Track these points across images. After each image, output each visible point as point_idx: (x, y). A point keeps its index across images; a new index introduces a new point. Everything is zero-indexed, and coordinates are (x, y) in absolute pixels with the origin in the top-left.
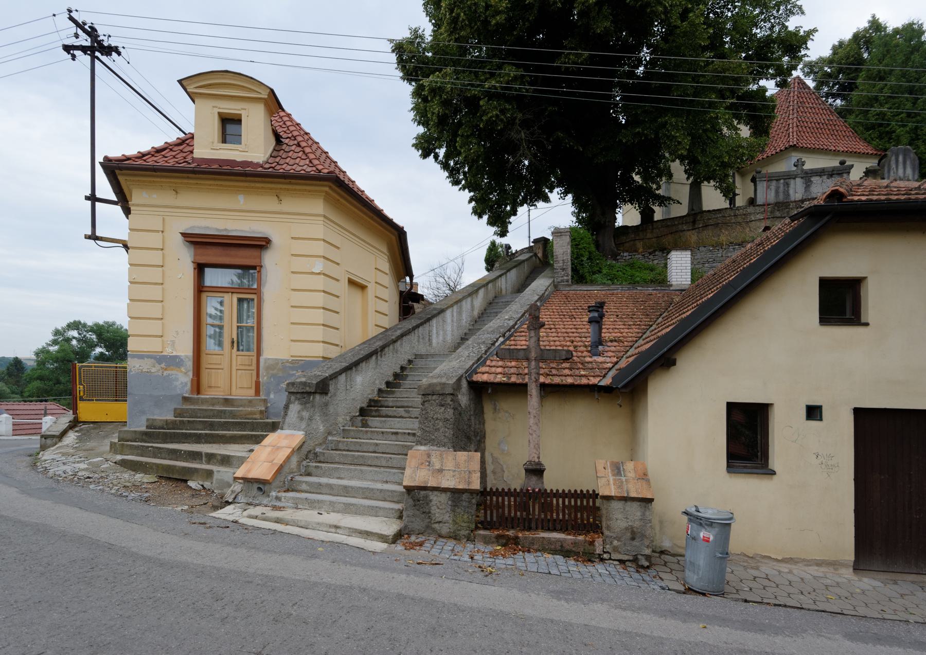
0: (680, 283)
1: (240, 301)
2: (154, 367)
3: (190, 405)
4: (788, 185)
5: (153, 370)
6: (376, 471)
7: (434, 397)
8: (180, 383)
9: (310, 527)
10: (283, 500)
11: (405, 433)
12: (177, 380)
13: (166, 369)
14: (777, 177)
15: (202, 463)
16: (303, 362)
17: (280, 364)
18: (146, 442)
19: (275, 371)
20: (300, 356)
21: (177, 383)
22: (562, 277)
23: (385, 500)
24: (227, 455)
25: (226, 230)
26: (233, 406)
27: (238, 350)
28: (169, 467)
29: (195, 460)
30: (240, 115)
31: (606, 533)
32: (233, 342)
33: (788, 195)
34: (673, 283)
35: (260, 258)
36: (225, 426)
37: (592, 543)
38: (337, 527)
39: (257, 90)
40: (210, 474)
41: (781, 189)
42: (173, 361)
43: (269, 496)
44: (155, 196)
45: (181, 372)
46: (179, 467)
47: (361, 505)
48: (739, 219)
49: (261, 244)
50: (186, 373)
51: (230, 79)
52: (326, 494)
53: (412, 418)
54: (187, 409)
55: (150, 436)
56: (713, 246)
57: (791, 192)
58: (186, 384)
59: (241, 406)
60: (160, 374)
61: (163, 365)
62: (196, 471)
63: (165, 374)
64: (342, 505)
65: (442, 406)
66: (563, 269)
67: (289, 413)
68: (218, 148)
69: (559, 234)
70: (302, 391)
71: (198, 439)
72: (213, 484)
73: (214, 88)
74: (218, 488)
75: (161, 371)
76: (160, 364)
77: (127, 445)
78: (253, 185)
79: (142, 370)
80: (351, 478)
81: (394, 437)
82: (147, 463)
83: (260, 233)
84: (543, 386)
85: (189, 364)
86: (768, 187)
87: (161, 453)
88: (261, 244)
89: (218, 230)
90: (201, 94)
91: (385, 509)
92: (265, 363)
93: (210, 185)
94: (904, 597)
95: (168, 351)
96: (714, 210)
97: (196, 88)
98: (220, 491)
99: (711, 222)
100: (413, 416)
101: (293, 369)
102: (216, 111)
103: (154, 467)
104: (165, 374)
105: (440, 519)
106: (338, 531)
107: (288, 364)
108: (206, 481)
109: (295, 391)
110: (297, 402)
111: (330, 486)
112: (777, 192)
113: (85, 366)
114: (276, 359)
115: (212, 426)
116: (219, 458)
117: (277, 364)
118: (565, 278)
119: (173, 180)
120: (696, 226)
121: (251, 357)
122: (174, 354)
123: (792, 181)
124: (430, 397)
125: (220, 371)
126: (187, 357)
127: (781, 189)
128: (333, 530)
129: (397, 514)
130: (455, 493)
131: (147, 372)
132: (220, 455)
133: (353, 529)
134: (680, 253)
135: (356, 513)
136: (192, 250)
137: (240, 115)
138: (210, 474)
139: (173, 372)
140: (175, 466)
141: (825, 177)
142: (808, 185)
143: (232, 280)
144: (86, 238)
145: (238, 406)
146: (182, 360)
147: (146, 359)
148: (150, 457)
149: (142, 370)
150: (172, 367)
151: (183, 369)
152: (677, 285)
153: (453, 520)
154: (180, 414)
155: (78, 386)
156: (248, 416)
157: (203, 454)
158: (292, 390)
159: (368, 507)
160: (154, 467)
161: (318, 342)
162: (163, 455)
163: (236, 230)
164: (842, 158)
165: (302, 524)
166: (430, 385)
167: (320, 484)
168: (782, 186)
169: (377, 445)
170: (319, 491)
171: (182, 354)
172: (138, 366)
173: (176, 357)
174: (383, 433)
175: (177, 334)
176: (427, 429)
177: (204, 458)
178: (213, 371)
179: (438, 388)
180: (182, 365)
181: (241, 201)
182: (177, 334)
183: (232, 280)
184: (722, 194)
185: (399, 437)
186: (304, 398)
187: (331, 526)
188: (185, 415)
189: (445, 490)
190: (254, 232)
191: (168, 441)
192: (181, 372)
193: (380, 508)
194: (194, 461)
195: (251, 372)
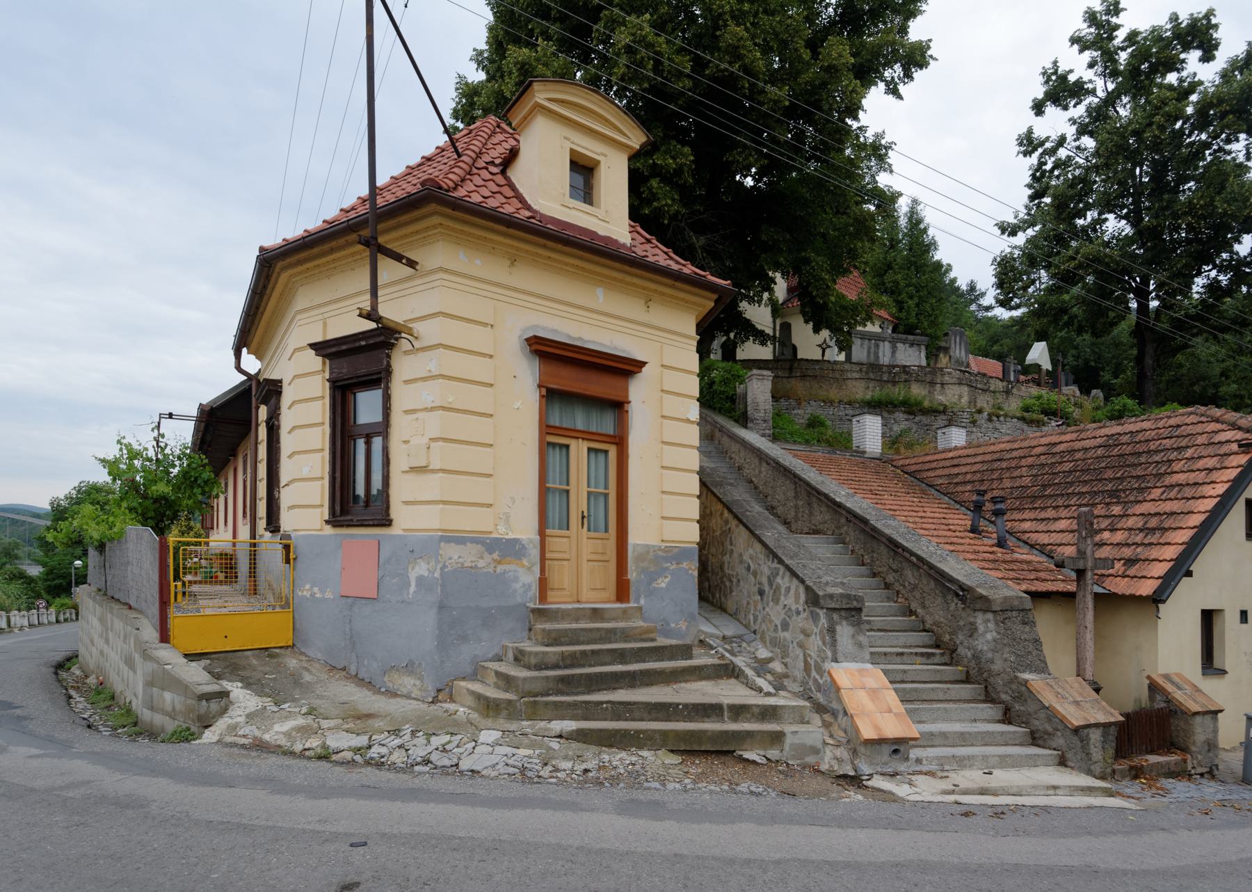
1: (589, 449)
2: (482, 558)
3: (546, 622)
4: (877, 346)
5: (481, 564)
6: (962, 709)
7: (1015, 614)
8: (521, 584)
9: (1024, 793)
10: (924, 762)
11: (911, 653)
12: (516, 579)
13: (499, 562)
15: (724, 722)
16: (675, 550)
17: (651, 553)
18: (563, 693)
19: (646, 564)
20: (674, 542)
21: (518, 586)
23: (1007, 745)
24: (771, 706)
25: (580, 339)
26: (603, 620)
27: (589, 530)
28: (692, 734)
29: (708, 717)
30: (598, 162)
31: (1193, 749)
32: (583, 517)
33: (878, 357)
35: (626, 390)
36: (640, 655)
37: (1185, 761)
38: (1055, 788)
39: (626, 131)
40: (777, 738)
42: (509, 549)
43: (907, 759)
44: (478, 262)
45: (523, 566)
46: (713, 732)
47: (1019, 755)
48: (837, 375)
49: (626, 368)
50: (529, 569)
51: (594, 103)
52: (940, 746)
53: (874, 630)
54: (566, 630)
55: (569, 683)
56: (824, 401)
57: (881, 354)
58: (530, 586)
59: (613, 619)
60: (491, 570)
61: (496, 556)
62: (750, 734)
63: (498, 570)
64: (997, 758)
65: (1026, 624)
66: (765, 421)
67: (838, 637)
68: (571, 206)
70: (848, 606)
71: (633, 680)
72: (785, 753)
73: (569, 108)
74: (794, 757)
75: (492, 565)
76: (491, 554)
77: (547, 703)
78: (629, 279)
79: (462, 564)
80: (934, 721)
81: (898, 659)
82: (638, 732)
83: (624, 351)
84: (1097, 596)
85: (535, 553)
86: (862, 345)
87: (631, 711)
88: (626, 368)
89: (570, 337)
90: (550, 111)
91: (1043, 755)
92: (634, 551)
93: (567, 264)
95: (502, 532)
96: (812, 360)
97: (550, 100)
98: (798, 762)
99: (810, 373)
100: (875, 628)
101: (667, 559)
102: (568, 145)
103: (657, 736)
104: (498, 570)
106: (1058, 792)
107: (661, 553)
108: (771, 748)
109: (837, 606)
110: (844, 623)
111: (944, 735)
112: (869, 352)
113: (188, 544)
114: (647, 546)
115: (621, 656)
116: (756, 710)
117: (648, 552)
119: (516, 244)
120: (794, 374)
121: (605, 541)
122: (511, 536)
123: (881, 344)
124: (1009, 614)
125: (565, 563)
126: (531, 541)
128: (1051, 792)
129: (1057, 761)
130: (1106, 726)
131: (471, 567)
132: (758, 706)
133: (1074, 786)
135: (1013, 767)
136: (536, 362)
137: (598, 162)
138: (777, 738)
139: (512, 567)
140: (704, 732)
141: (907, 345)
144: (360, 315)
145: (609, 621)
146: (523, 546)
147: (468, 544)
148: (606, 720)
149: (462, 564)
150: (509, 558)
151: (525, 562)
152: (871, 452)
154: (556, 640)
155: (173, 584)
156: (644, 636)
157: (725, 707)
158: (833, 606)
159: (1026, 755)
160: (657, 736)
161: (687, 520)
162: (637, 714)
163: (594, 342)
165: (1014, 790)
166: (1006, 598)
167: (932, 734)
169: (905, 671)
170: (931, 743)
171: (524, 537)
172: (456, 557)
173: (516, 541)
174: (885, 654)
175: (514, 502)
176: (1019, 652)
177: (726, 713)
178: (555, 562)
179: (1016, 603)
180: (524, 555)
181: (600, 297)
182: (514, 502)
185: (905, 658)
186: (853, 616)
187: (1048, 788)
188: (563, 640)
189: (1097, 725)
190: (616, 348)
191: (593, 688)
192: (523, 566)
193: (1038, 755)
194: (706, 720)
195: (605, 564)
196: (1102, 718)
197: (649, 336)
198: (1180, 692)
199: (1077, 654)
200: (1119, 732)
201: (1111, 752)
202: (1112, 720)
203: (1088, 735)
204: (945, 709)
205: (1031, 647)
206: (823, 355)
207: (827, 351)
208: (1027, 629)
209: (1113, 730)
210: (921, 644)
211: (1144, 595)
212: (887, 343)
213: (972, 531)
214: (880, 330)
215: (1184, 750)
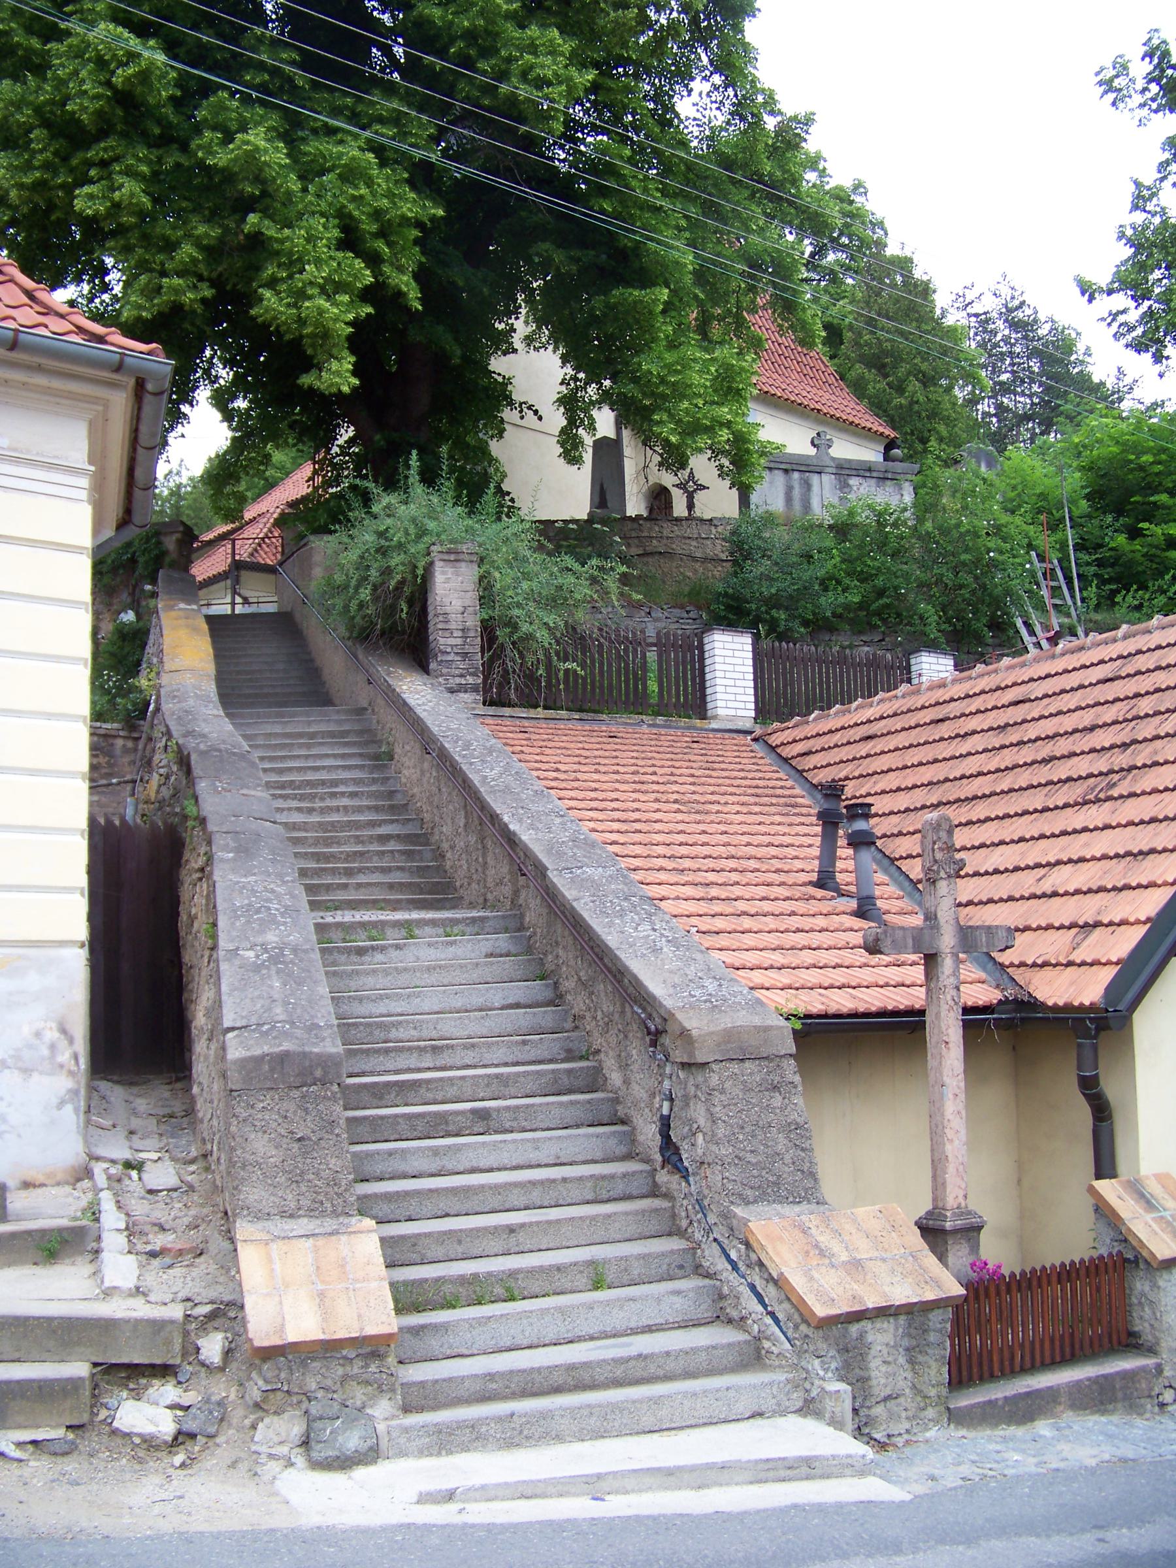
0: (732, 712)
4: (808, 486)
14: (1160, 463)
22: (462, 676)
34: (720, 712)
41: (797, 493)
65: (775, 1088)
69: (452, 557)
94: (417, 932)
105: (888, 1392)
118: (470, 679)
123: (815, 479)
127: (797, 493)
130: (914, 1312)
134: (729, 638)
142: (844, 486)
143: (171, 1407)
153: (914, 1387)
164: (821, 429)
168: (796, 485)
183: (171, 1407)
184: (727, 483)
189: (883, 1312)
196: (902, 1293)
197: (23, 484)
198: (1149, 1217)
199: (932, 1150)
200: (957, 1321)
201: (937, 1371)
202: (930, 1295)
203: (862, 1335)
204: (560, 1310)
205: (781, 1144)
206: (744, 501)
207: (699, 497)
208: (777, 1101)
209: (941, 1321)
210: (599, 1155)
211: (1087, 1003)
212: (825, 477)
213: (820, 884)
214: (813, 451)
215: (1151, 1351)
